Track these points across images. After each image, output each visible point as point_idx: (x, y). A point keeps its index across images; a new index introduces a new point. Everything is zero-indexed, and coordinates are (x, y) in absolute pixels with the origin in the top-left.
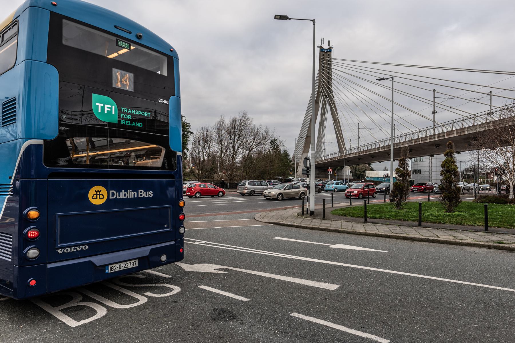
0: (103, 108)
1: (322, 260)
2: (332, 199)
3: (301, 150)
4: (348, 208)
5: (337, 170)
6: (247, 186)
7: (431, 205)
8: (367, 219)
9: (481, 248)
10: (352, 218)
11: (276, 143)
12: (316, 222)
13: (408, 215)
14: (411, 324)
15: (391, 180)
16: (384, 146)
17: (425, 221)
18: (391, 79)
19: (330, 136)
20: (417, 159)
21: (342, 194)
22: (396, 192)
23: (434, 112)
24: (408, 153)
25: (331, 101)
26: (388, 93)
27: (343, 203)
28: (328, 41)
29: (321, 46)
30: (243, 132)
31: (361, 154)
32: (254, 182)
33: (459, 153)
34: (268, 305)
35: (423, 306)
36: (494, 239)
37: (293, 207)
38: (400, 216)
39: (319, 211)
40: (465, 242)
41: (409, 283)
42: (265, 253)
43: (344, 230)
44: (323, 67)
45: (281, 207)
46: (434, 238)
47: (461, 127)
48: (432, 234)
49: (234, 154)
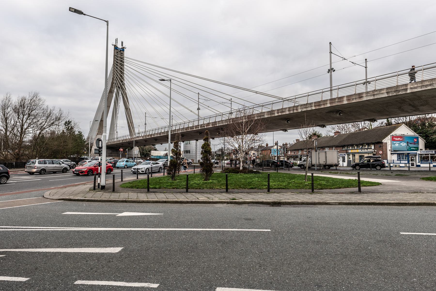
1: (109, 228)
2: (122, 175)
3: (96, 132)
4: (135, 181)
5: (127, 150)
6: (37, 164)
7: (194, 176)
8: (150, 189)
9: (224, 204)
10: (137, 190)
11: (71, 125)
12: (106, 195)
13: (179, 184)
14: (175, 267)
15: (169, 157)
16: (164, 132)
17: (191, 188)
18: (170, 81)
19: (122, 121)
20: (187, 142)
21: (129, 170)
22: (172, 167)
23: (199, 109)
24: (180, 138)
25: (124, 92)
26: (167, 91)
27: (132, 177)
28: (122, 42)
29: (116, 44)
30: (34, 111)
31: (147, 137)
32: (45, 160)
33: (213, 139)
34: (51, 279)
35: (185, 252)
36: (231, 197)
37: (86, 183)
38: (174, 186)
39: (110, 185)
40: (214, 201)
41: (177, 236)
42: (52, 229)
43: (130, 200)
44: (117, 62)
45: (73, 184)
46: (196, 200)
47: (214, 121)
48: (194, 198)
49: (23, 132)
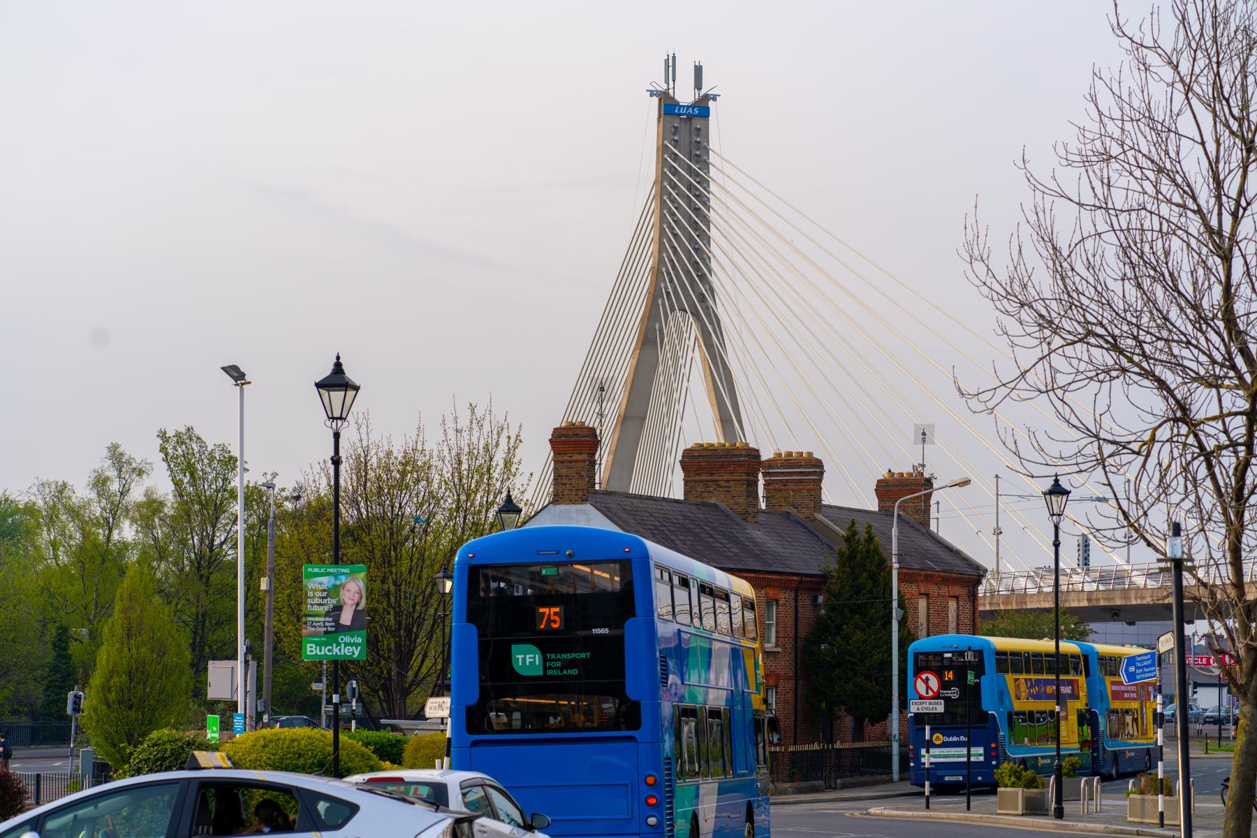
0: (524, 660)
28: (696, 66)
